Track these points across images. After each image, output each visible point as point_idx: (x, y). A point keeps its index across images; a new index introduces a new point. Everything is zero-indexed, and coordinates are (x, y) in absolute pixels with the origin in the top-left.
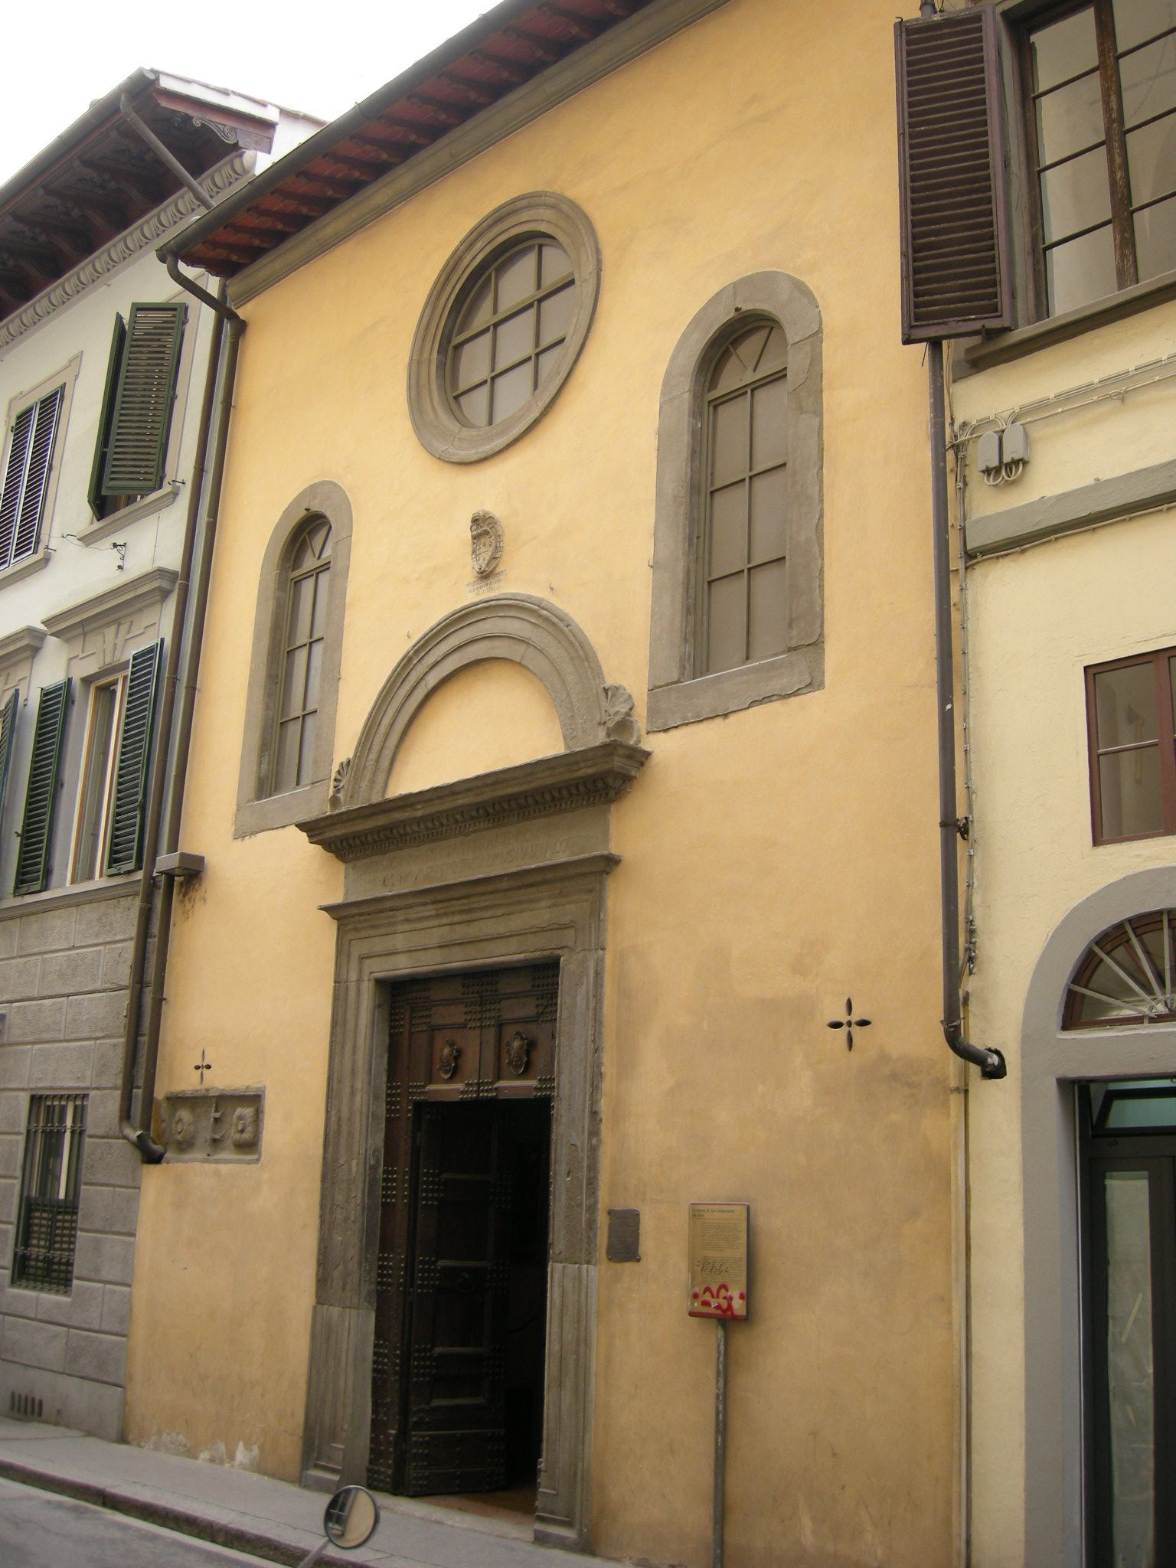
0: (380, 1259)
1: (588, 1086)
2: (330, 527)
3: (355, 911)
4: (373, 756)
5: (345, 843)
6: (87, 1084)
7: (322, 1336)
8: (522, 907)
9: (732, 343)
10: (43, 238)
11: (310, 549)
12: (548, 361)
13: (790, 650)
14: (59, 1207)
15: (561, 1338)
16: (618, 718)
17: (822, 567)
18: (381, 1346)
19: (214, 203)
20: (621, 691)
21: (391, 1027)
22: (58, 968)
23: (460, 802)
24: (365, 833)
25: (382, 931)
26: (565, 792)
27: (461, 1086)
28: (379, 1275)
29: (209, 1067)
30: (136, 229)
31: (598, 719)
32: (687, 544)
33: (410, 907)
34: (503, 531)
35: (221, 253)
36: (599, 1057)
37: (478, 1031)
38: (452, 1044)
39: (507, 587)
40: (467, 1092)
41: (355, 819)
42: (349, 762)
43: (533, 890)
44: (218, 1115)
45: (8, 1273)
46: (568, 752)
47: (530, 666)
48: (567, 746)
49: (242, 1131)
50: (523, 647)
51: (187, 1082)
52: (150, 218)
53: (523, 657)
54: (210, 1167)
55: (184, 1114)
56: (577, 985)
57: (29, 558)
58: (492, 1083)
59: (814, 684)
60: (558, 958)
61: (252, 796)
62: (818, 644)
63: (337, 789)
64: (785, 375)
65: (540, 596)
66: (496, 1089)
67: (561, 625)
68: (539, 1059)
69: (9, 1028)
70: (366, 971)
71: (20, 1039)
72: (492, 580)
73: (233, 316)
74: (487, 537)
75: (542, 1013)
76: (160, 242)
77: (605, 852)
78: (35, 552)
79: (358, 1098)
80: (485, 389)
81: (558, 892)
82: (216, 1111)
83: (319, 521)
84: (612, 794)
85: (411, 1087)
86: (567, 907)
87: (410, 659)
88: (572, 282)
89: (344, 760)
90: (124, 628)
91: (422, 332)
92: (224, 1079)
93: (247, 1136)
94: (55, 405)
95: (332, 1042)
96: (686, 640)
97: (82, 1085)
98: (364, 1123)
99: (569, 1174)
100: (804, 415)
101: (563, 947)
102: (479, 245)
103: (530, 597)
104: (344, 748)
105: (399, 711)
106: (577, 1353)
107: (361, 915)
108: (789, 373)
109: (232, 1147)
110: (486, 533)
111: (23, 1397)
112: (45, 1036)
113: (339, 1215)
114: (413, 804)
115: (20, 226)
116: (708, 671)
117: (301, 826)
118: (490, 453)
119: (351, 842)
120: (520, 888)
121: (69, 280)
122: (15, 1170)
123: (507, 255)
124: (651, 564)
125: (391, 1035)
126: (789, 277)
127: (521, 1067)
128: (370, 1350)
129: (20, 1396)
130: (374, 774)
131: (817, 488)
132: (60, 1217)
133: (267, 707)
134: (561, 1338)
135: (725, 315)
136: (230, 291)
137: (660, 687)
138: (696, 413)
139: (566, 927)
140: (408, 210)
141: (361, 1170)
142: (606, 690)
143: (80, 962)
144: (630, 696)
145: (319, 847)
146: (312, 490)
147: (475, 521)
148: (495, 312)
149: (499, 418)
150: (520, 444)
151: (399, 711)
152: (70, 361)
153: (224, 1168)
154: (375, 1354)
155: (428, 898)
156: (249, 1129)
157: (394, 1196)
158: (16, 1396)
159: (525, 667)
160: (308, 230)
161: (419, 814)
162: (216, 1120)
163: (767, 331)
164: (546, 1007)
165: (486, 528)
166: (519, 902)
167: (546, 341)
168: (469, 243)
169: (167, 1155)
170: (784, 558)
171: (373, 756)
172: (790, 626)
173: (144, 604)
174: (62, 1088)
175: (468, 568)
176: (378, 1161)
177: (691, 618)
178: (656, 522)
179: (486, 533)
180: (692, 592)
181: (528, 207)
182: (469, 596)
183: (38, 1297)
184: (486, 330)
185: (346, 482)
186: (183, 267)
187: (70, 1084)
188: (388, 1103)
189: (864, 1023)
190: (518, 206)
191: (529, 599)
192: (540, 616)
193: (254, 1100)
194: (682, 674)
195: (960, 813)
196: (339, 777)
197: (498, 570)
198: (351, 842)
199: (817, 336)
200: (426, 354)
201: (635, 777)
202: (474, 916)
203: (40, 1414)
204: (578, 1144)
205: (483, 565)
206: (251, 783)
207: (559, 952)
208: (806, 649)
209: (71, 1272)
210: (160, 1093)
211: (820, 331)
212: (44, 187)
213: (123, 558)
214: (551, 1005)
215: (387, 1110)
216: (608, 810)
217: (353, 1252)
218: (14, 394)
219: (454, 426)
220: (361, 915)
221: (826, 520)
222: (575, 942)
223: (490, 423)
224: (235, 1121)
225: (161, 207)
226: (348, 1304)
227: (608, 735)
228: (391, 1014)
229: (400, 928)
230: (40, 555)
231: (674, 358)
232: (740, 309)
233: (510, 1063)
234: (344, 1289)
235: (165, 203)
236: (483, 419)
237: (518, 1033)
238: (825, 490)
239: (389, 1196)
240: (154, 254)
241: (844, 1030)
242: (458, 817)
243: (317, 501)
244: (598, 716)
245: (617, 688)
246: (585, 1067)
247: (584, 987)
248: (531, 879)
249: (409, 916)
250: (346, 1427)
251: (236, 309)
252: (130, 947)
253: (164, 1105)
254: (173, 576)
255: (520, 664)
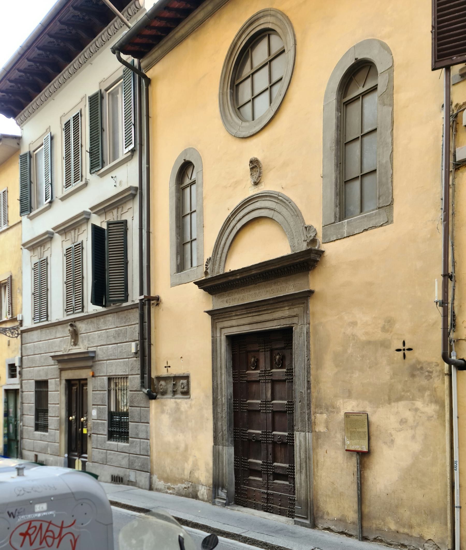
0: (234, 429)
1: (306, 372)
2: (194, 166)
3: (217, 312)
4: (219, 256)
5: (211, 288)
6: (128, 374)
7: (217, 456)
8: (278, 310)
9: (353, 75)
10: (62, 44)
11: (186, 175)
12: (276, 89)
13: (379, 208)
14: (122, 414)
15: (300, 457)
16: (311, 238)
17: (393, 173)
18: (237, 458)
19: (131, 25)
20: (312, 227)
21: (232, 352)
22: (112, 334)
23: (253, 273)
24: (219, 285)
25: (221, 320)
26: (292, 268)
27: (259, 371)
28: (234, 435)
29: (169, 367)
30: (99, 37)
31: (303, 239)
32: (336, 167)
33: (237, 310)
34: (262, 165)
35: (137, 48)
36: (309, 362)
37: (264, 352)
38: (255, 357)
39: (264, 188)
40: (261, 373)
41: (215, 280)
42: (210, 258)
43: (282, 303)
44: (174, 383)
45: (106, 437)
46: (293, 253)
47: (276, 219)
48: (293, 251)
49: (183, 388)
50: (273, 212)
51: (163, 373)
52: (104, 32)
53: (273, 216)
54: (173, 400)
55: (163, 383)
56: (300, 337)
57: (79, 184)
58: (270, 370)
59: (388, 222)
60: (292, 327)
61: (175, 272)
62: (391, 205)
63: (207, 269)
64: (376, 88)
65: (278, 191)
66: (271, 372)
67: (287, 202)
68: (287, 363)
69: (98, 355)
70: (223, 333)
71: (102, 359)
72: (259, 185)
73: (145, 77)
74: (256, 168)
75: (287, 346)
76: (112, 45)
77: (309, 289)
78: (82, 181)
79: (223, 377)
80: (250, 104)
81: (291, 304)
82: (173, 381)
83: (190, 164)
84: (310, 268)
85: (241, 372)
86: (295, 309)
87: (230, 218)
88: (284, 51)
89: (209, 258)
90: (120, 210)
91: (223, 80)
92: (175, 371)
93: (185, 389)
94: (79, 118)
95: (212, 358)
96: (337, 206)
97: (126, 374)
98: (226, 385)
99: (300, 402)
100: (385, 106)
101: (294, 324)
102: (243, 36)
103: (275, 192)
104: (208, 254)
105: (227, 239)
106: (306, 462)
107: (219, 313)
108: (379, 87)
109: (180, 393)
110: (256, 166)
111: (116, 476)
112: (111, 358)
113: (220, 415)
114: (236, 274)
115: (52, 40)
116: (345, 217)
117: (195, 283)
118: (255, 132)
119: (214, 288)
120: (277, 303)
121: (75, 62)
122: (105, 403)
123: (255, 40)
124: (322, 176)
125: (233, 355)
126: (379, 41)
127: (280, 365)
128: (233, 459)
129: (114, 476)
130: (220, 263)
131: (391, 139)
132: (123, 418)
133: (177, 238)
134: (300, 457)
135: (350, 62)
136: (142, 65)
137: (327, 225)
138: (339, 109)
139: (295, 316)
140: (211, 22)
141: (226, 400)
142: (306, 228)
143: (120, 332)
144: (315, 229)
145: (202, 290)
146: (185, 152)
147: (251, 162)
148: (252, 68)
149: (257, 117)
150: (267, 128)
151: (227, 239)
152: (82, 99)
153: (179, 401)
154: (235, 461)
155: (243, 307)
156: (186, 387)
157: (238, 409)
158: (113, 476)
159: (274, 220)
160: (171, 35)
161: (238, 277)
162: (174, 384)
163: (369, 67)
164: (288, 344)
165: (255, 164)
166: (277, 308)
167: (274, 80)
168: (239, 36)
169: (158, 396)
170: (376, 170)
171: (219, 256)
172: (379, 199)
173: (126, 200)
174: (119, 375)
175: (249, 181)
176: (231, 397)
177: (338, 197)
178: (323, 159)
179: (256, 166)
180: (338, 186)
181: (263, 16)
182: (252, 191)
183: (118, 445)
184: (249, 77)
185: (199, 148)
186: (122, 55)
187: (122, 374)
188: (233, 378)
189: (410, 349)
190: (259, 16)
191: (275, 192)
192: (279, 199)
193: (187, 377)
194: (335, 220)
195: (450, 270)
196: (207, 264)
197: (261, 181)
198: (214, 288)
199: (391, 69)
200: (225, 90)
201: (318, 261)
202: (261, 313)
203: (122, 481)
204: (303, 392)
205: (256, 180)
206: (175, 267)
207: (293, 325)
208: (386, 208)
209: (128, 436)
210: (153, 375)
211: (392, 66)
212: (60, 21)
213: (116, 182)
214: (290, 343)
215: (233, 380)
216: (309, 273)
217: (225, 428)
218: (61, 114)
219: (239, 122)
220: (219, 313)
221: (394, 152)
222: (298, 322)
223: (253, 119)
224: (180, 385)
225: (108, 27)
226: (225, 445)
227: (308, 245)
228: (232, 347)
229: (234, 318)
230: (84, 182)
231: (329, 84)
232: (357, 58)
233: (276, 363)
234: (223, 440)
235: (110, 24)
236: (251, 118)
237: (278, 353)
238: (394, 140)
239: (236, 409)
240: (110, 50)
241: (402, 352)
242: (253, 278)
243: (188, 155)
244: (303, 237)
245: (310, 227)
246: (304, 365)
247: (303, 338)
248: (281, 300)
249: (237, 314)
250: (227, 485)
251: (146, 73)
252: (137, 327)
253: (155, 380)
254: (136, 189)
255: (272, 219)
